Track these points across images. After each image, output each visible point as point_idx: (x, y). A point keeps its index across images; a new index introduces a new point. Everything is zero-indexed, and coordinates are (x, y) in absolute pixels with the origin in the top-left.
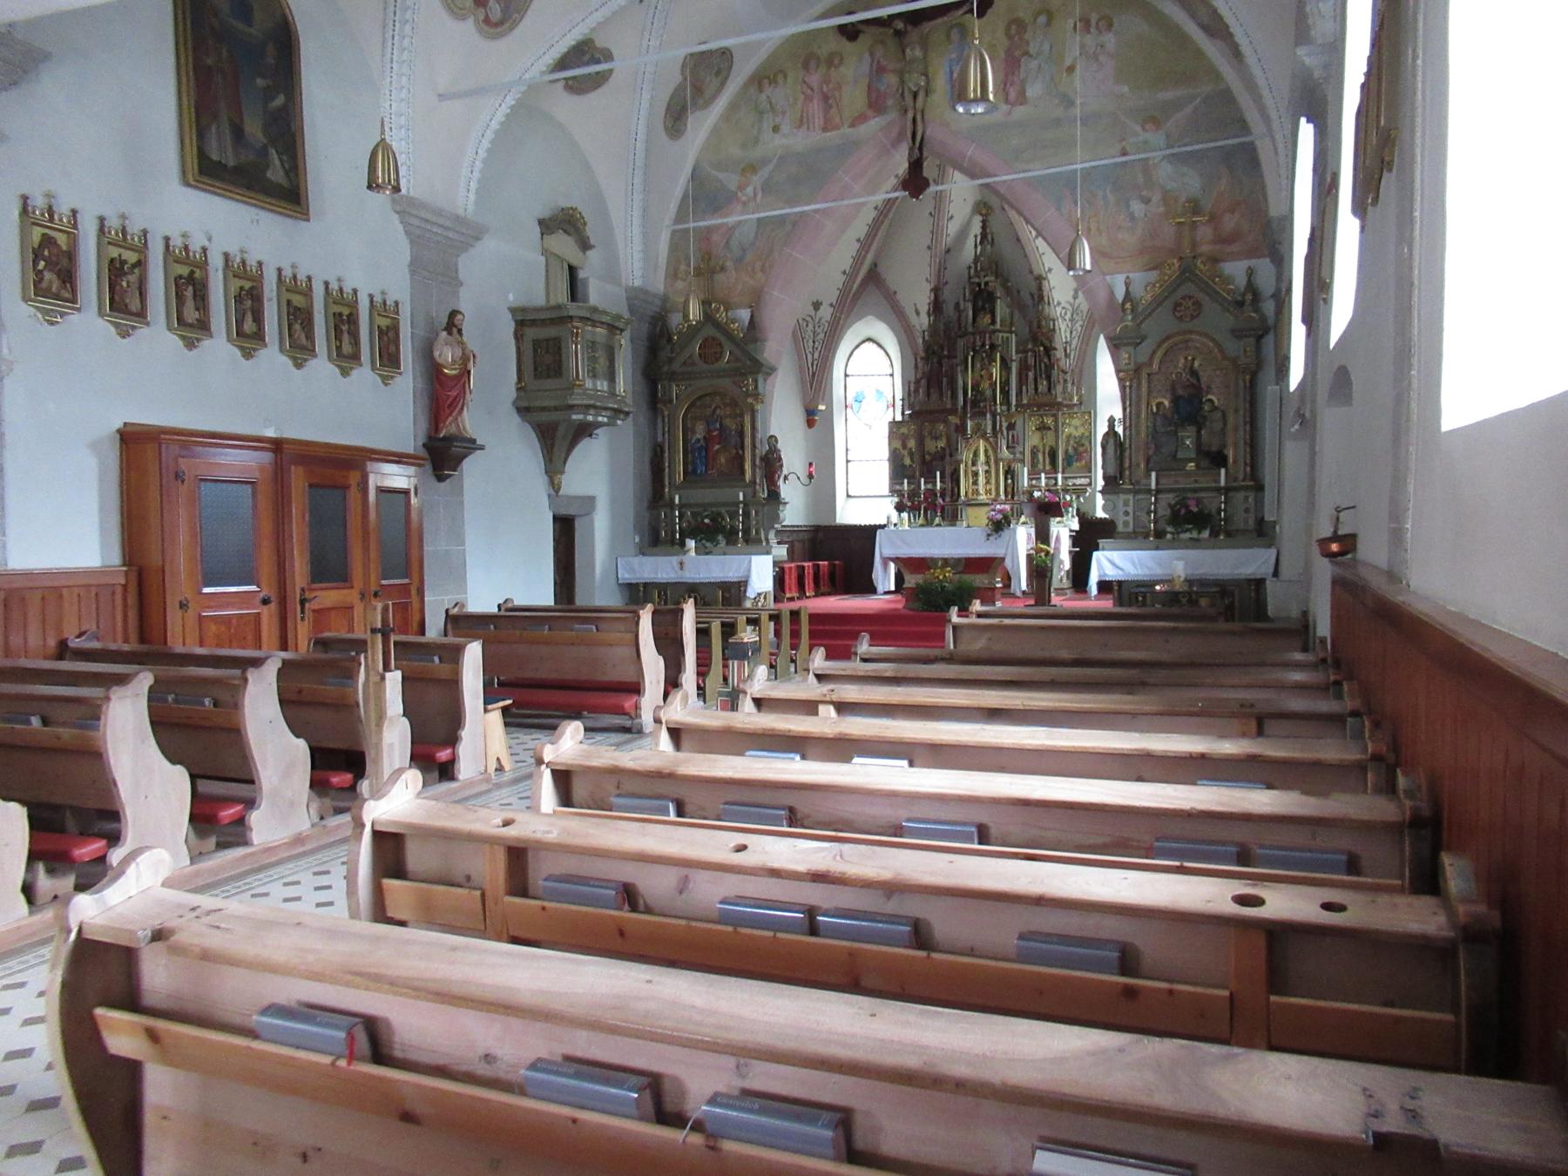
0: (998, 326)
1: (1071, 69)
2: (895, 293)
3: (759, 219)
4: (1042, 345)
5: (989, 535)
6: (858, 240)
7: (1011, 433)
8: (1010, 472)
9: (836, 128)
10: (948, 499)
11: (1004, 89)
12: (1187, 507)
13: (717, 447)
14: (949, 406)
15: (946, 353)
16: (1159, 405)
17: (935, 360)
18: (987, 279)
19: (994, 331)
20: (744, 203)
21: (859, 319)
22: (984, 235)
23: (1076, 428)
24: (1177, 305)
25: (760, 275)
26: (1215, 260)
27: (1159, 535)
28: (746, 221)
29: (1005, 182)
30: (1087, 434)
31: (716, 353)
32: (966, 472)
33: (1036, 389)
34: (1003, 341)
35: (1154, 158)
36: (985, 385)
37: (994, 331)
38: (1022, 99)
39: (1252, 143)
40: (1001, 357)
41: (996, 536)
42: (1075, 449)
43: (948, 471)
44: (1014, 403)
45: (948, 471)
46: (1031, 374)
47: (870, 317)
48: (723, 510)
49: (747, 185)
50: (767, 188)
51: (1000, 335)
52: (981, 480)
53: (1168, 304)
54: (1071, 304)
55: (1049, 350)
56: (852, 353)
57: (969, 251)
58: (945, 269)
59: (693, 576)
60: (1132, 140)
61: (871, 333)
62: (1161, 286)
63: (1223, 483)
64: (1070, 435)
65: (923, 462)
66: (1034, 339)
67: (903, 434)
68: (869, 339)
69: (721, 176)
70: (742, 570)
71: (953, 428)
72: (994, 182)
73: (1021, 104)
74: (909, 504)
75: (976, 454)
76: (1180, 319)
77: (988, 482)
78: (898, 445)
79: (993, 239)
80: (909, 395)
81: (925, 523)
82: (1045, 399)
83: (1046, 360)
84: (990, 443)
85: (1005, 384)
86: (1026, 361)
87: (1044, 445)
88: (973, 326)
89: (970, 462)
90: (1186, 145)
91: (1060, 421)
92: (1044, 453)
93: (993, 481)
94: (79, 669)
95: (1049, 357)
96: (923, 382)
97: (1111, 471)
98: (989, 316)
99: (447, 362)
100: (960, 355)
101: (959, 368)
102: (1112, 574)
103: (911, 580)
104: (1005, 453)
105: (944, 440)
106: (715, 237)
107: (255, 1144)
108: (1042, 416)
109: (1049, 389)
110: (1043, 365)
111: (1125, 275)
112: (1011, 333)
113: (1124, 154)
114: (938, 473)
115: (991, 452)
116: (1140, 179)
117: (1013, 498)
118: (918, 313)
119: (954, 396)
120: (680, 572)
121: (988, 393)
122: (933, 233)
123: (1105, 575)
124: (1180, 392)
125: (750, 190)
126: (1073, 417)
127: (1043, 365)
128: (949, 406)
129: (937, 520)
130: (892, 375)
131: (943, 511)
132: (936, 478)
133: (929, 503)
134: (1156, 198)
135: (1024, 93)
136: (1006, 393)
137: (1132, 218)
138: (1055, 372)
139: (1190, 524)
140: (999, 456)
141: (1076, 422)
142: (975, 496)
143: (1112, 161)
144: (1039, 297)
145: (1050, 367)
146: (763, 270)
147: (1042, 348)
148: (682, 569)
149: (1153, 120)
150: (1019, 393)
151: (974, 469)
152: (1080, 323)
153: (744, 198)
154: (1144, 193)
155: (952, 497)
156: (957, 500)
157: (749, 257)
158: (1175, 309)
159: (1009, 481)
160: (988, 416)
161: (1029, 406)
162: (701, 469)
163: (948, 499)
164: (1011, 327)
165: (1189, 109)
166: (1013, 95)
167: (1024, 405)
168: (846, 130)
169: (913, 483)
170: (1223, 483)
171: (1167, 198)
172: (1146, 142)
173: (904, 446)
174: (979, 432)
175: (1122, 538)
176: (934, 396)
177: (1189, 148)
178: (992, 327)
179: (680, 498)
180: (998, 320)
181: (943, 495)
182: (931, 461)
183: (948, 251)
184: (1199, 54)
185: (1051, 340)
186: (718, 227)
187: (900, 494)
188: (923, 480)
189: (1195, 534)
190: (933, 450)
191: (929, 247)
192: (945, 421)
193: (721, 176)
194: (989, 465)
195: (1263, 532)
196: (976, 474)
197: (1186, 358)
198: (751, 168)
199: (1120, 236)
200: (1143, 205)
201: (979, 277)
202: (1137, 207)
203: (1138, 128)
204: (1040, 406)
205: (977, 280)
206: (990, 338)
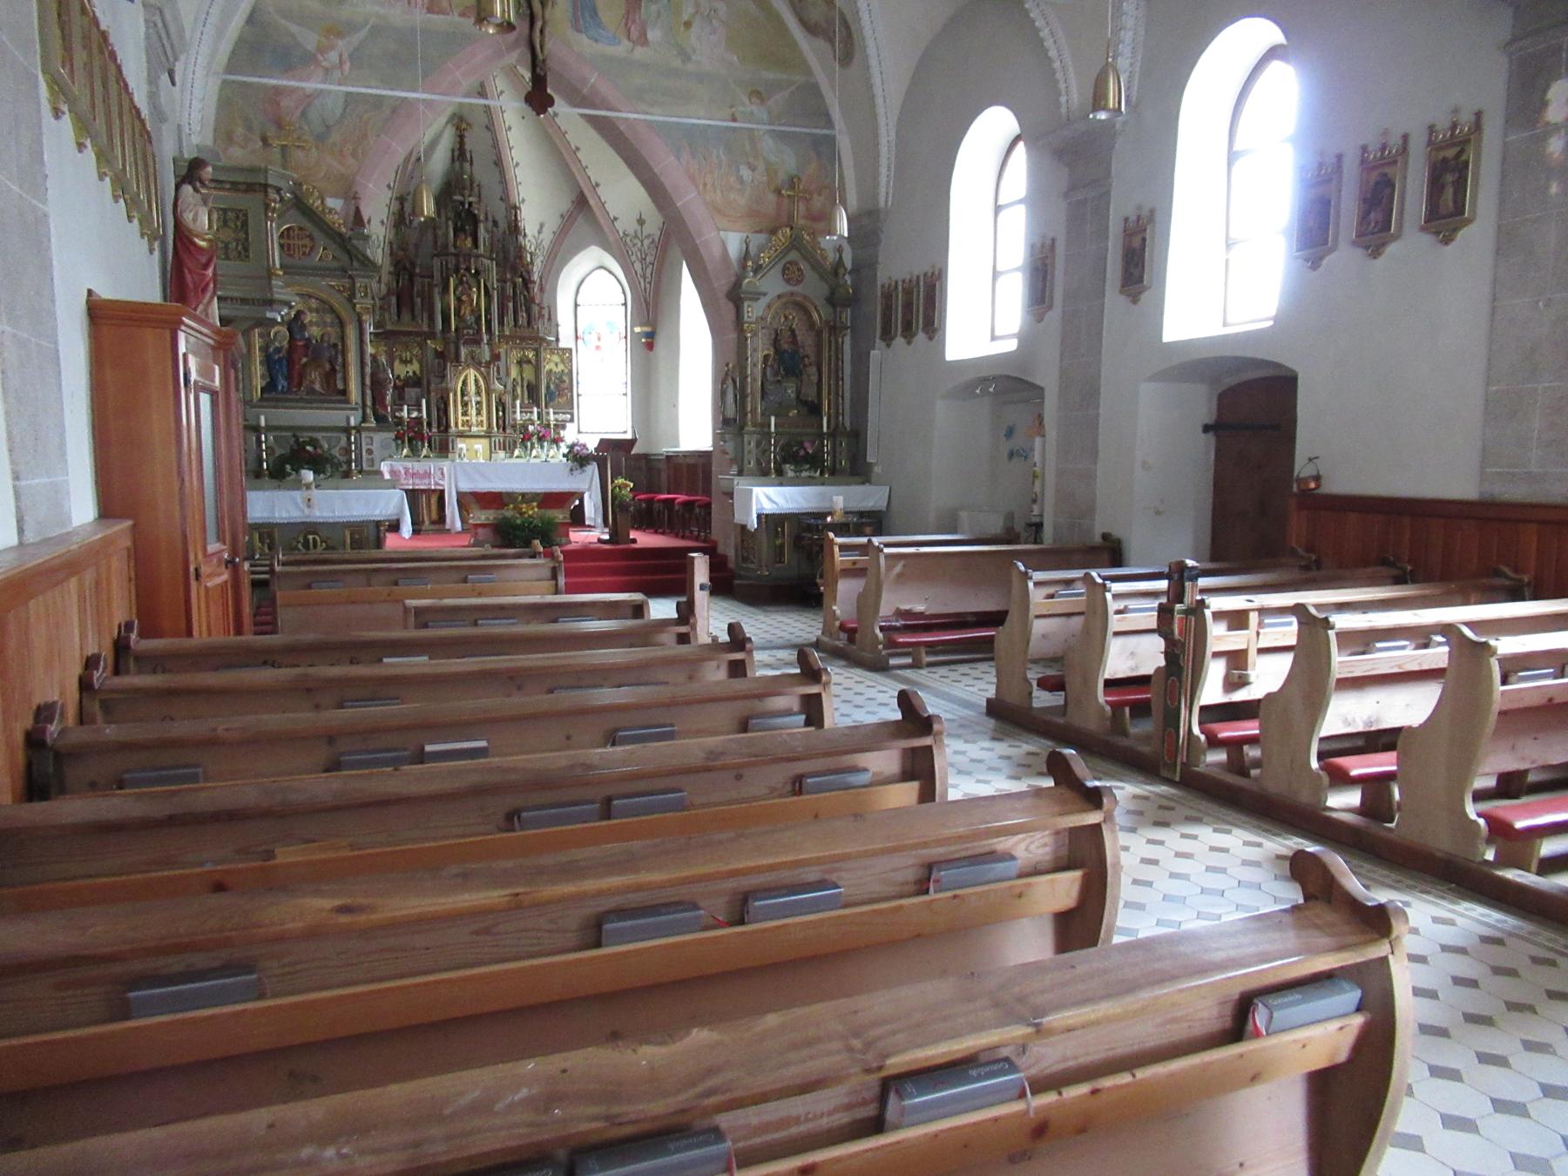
0: (481, 250)
1: (688, 25)
3: (348, 94)
4: (521, 276)
5: (571, 470)
8: (501, 404)
9: (442, 12)
10: (434, 430)
11: (626, 24)
12: (805, 449)
13: (304, 360)
14: (425, 328)
15: (418, 271)
17: (407, 277)
20: (327, 70)
23: (556, 365)
24: (785, 269)
25: (350, 161)
26: (813, 234)
27: (780, 472)
28: (330, 92)
29: (626, 119)
31: (305, 246)
32: (455, 401)
33: (516, 320)
35: (758, 130)
37: (478, 256)
38: (643, 40)
39: (835, 136)
41: (579, 471)
46: (511, 305)
48: (319, 436)
49: (332, 48)
50: (356, 57)
53: (779, 267)
55: (527, 283)
57: (439, 163)
59: (325, 514)
60: (741, 109)
62: (776, 250)
63: (825, 430)
64: (551, 370)
66: (514, 270)
68: (601, 267)
69: (294, 28)
70: (392, 506)
71: (430, 355)
72: (618, 118)
73: (642, 45)
75: (465, 383)
76: (788, 281)
77: (479, 413)
82: (526, 333)
84: (481, 374)
86: (503, 289)
87: (522, 379)
88: (455, 246)
90: (783, 125)
91: (543, 354)
92: (522, 386)
93: (484, 411)
94: (454, 669)
95: (528, 289)
96: (394, 300)
97: (731, 411)
98: (469, 239)
99: (203, 229)
102: (769, 508)
103: (481, 516)
106: (285, 103)
107: (1269, 1098)
109: (529, 323)
111: (745, 235)
112: (492, 259)
113: (734, 120)
116: (748, 148)
117: (504, 429)
119: (431, 318)
120: (307, 511)
121: (470, 319)
123: (763, 509)
124: (786, 346)
125: (333, 56)
126: (553, 353)
128: (425, 328)
129: (425, 452)
134: (761, 167)
135: (645, 34)
137: (742, 181)
138: (535, 309)
139: (807, 463)
140: (492, 387)
141: (556, 358)
142: (466, 428)
143: (725, 124)
144: (515, 229)
145: (529, 301)
146: (354, 155)
148: (309, 506)
149: (757, 95)
150: (501, 323)
151: (466, 398)
152: (541, 258)
153: (324, 64)
154: (751, 160)
155: (439, 427)
157: (335, 137)
158: (783, 273)
159: (501, 413)
162: (282, 383)
163: (434, 430)
165: (786, 93)
166: (635, 34)
168: (457, 19)
170: (825, 430)
171: (770, 170)
172: (752, 113)
174: (476, 363)
175: (748, 475)
176: (406, 317)
177: (782, 128)
179: (266, 420)
184: (793, 45)
185: (529, 272)
186: (293, 90)
189: (812, 474)
192: (422, 346)
193: (294, 28)
195: (858, 470)
196: (465, 405)
197: (786, 318)
198: (336, 31)
199: (732, 196)
200: (750, 172)
201: (463, 196)
202: (745, 173)
203: (747, 102)
204: (522, 339)
206: (475, 263)
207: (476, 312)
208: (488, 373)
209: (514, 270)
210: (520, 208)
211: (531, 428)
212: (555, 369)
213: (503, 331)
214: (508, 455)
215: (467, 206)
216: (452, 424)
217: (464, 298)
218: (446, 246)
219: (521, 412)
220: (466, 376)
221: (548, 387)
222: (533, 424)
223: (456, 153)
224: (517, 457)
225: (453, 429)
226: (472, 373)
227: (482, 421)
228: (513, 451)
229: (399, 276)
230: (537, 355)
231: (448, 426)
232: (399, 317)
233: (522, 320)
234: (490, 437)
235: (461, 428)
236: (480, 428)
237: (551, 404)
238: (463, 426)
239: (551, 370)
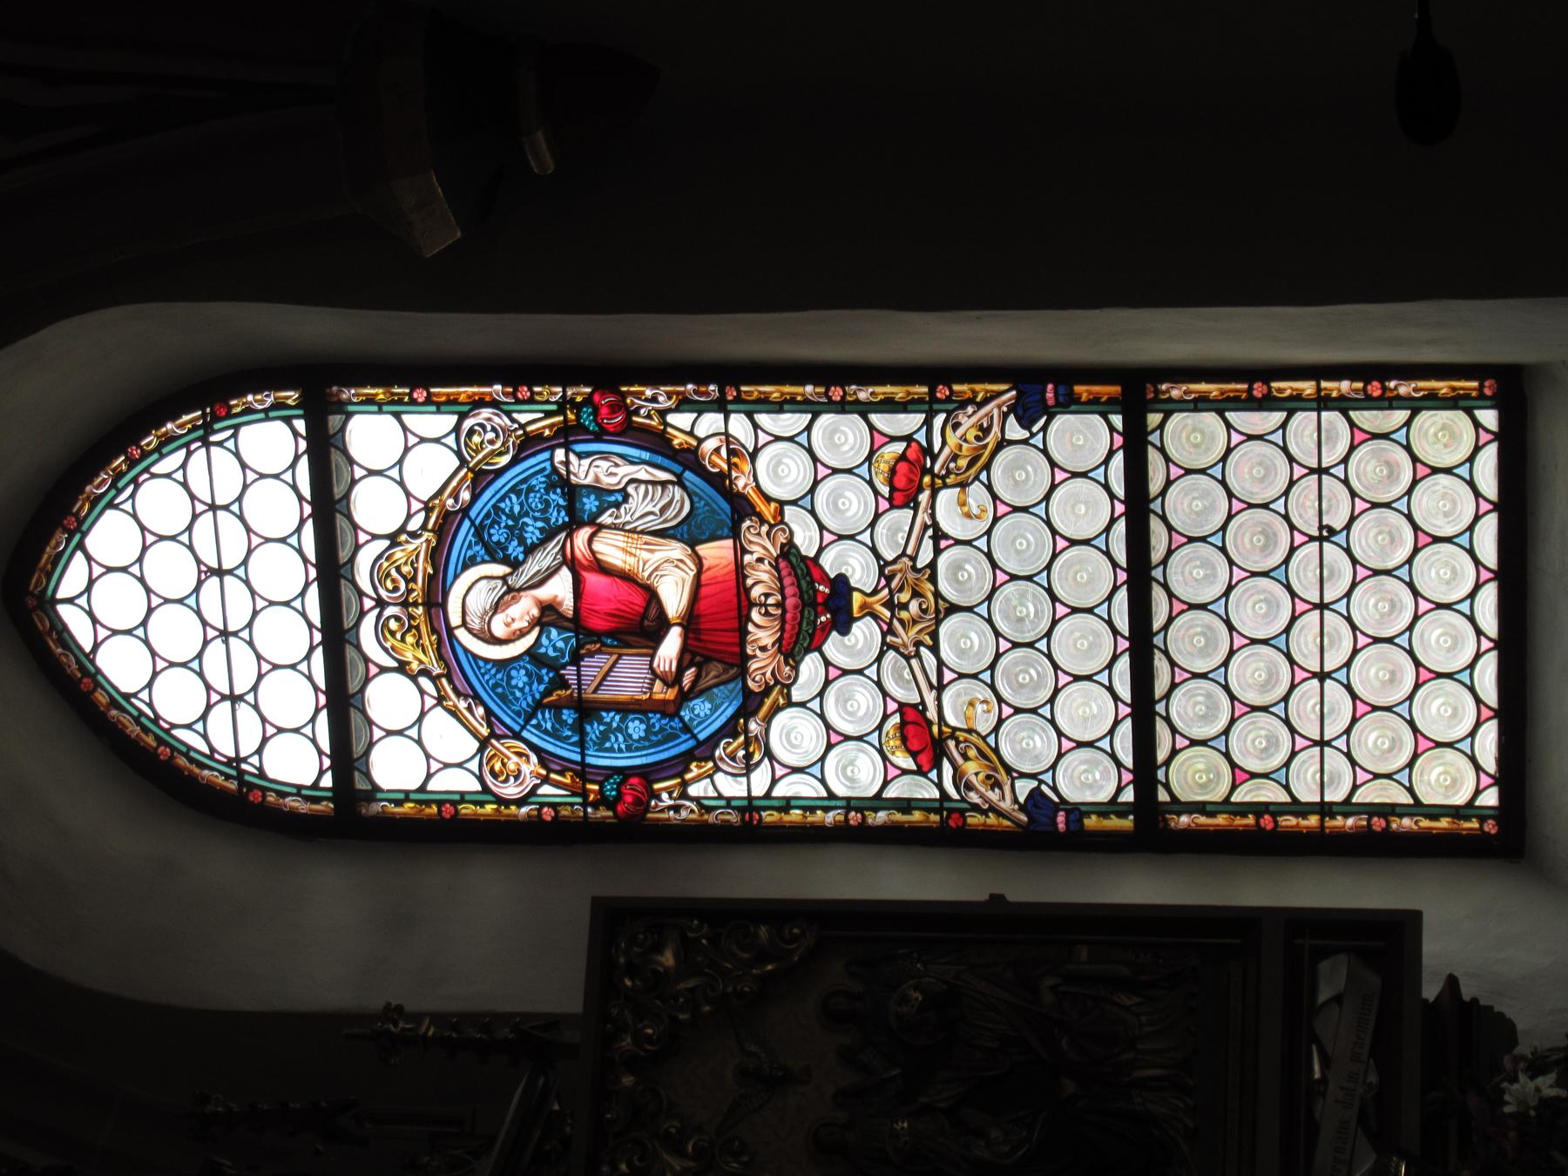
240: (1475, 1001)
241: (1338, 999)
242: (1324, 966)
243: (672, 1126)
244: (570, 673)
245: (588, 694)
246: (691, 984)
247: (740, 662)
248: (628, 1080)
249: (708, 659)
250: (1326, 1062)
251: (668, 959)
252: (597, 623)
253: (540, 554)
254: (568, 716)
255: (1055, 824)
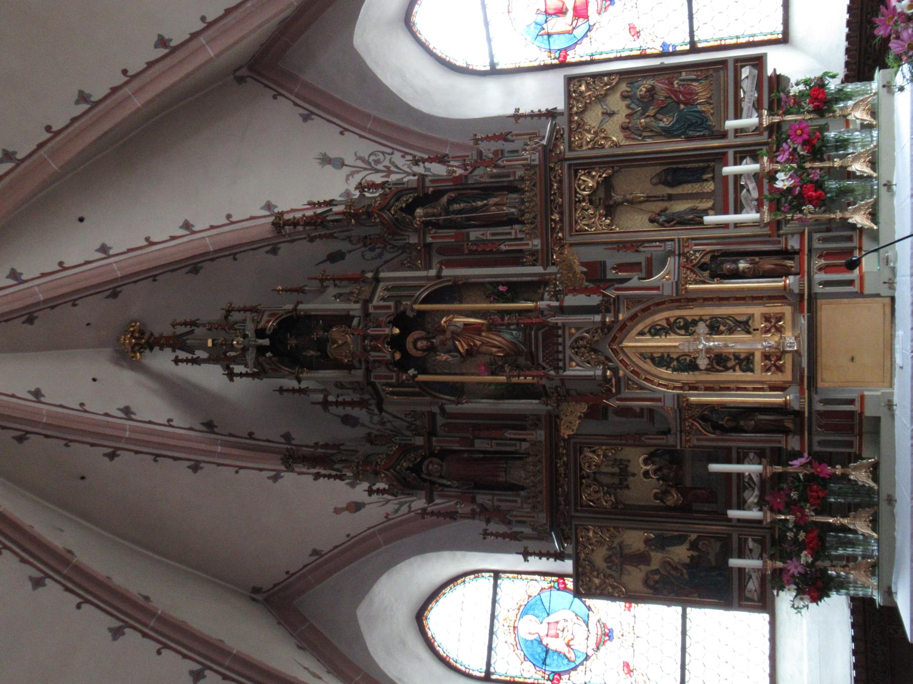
0: (355, 308)
2: (315, 552)
4: (410, 209)
6: (116, 633)
7: (611, 274)
10: (794, 443)
14: (540, 435)
15: (419, 441)
16: (680, 322)
18: (250, 332)
19: (367, 315)
21: (359, 639)
22: (176, 343)
23: (611, 114)
30: (624, 87)
32: (710, 388)
33: (511, 221)
34: (389, 298)
36: (499, 341)
37: (367, 315)
40: (425, 301)
42: (663, 110)
43: (711, 440)
44: (539, 269)
45: (711, 440)
46: (474, 234)
47: (361, 612)
51: (375, 302)
52: (738, 343)
54: (352, 174)
56: (444, 661)
58: (251, 435)
61: (403, 616)
64: (624, 128)
65: (684, 510)
66: (397, 227)
67: (608, 559)
68: (420, 617)
71: (595, 427)
74: (806, 557)
75: (663, 360)
77: (745, 325)
78: (635, 576)
79: (185, 324)
80: (514, 537)
81: (866, 514)
83: (445, 199)
85: (492, 291)
86: (443, 250)
87: (649, 199)
88: (350, 367)
89: (685, 377)
91: (585, 152)
92: (670, 198)
95: (438, 194)
96: (484, 498)
100: (423, 404)
101: (450, 408)
104: (665, 277)
105: (628, 453)
108: (575, 202)
109: (512, 189)
110: (456, 207)
112: (377, 280)
114: (714, 467)
115: (660, 317)
118: (356, 507)
119: (518, 422)
122: (157, 456)
127: (456, 207)
128: (540, 435)
129: (861, 476)
130: (497, 574)
131: (830, 459)
132: (728, 475)
133: (804, 498)
136: (516, 290)
138: (482, 175)
140: (668, 291)
142: (787, 361)
147: (419, 211)
150: (515, 258)
151: (703, 363)
152: (397, 158)
155: (786, 431)
156: (799, 414)
159: (742, 265)
160: (559, 320)
161: (548, 231)
163: (794, 443)
164: (365, 280)
167: (545, 243)
169: (742, 543)
173: (641, 559)
176: (518, 474)
178: (355, 322)
180: (340, 306)
181: (779, 456)
182: (683, 491)
183: (210, 426)
185: (400, 191)
187: (778, 580)
188: (733, 514)
190: (653, 485)
191: (195, 468)
194: (695, 323)
196: (719, 361)
204: (549, 205)
205: (251, 356)
206: (379, 326)
207: (494, 322)
208: (637, 300)
209: (397, 227)
210: (282, 213)
211: (783, 181)
212: (621, 118)
213: (533, 253)
214: (867, 245)
215: (266, 342)
216: (775, 398)
217: (462, 347)
218: (356, 387)
219: (737, 211)
220: (643, 356)
221: (668, 133)
222: (772, 177)
223: (182, 355)
224: (874, 216)
225: (790, 397)
226: (635, 342)
227: (767, 318)
228: (853, 227)
229: (433, 483)
230: (588, 165)
231: (782, 410)
232: (523, 488)
233: (508, 205)
234: (812, 297)
235: (787, 376)
236: (786, 323)
237: (712, 121)
238: (780, 369)
239: (624, 128)
240: (780, 75)
241: (747, 77)
242: (743, 70)
243: (587, 127)
244: (545, 26)
245: (550, 31)
246: (589, 93)
247: (586, 17)
248: (576, 118)
249: (579, 18)
250: (744, 92)
251: (583, 88)
252: (551, 12)
253: (444, 501)
254: (546, 37)
255: (207, 343)
